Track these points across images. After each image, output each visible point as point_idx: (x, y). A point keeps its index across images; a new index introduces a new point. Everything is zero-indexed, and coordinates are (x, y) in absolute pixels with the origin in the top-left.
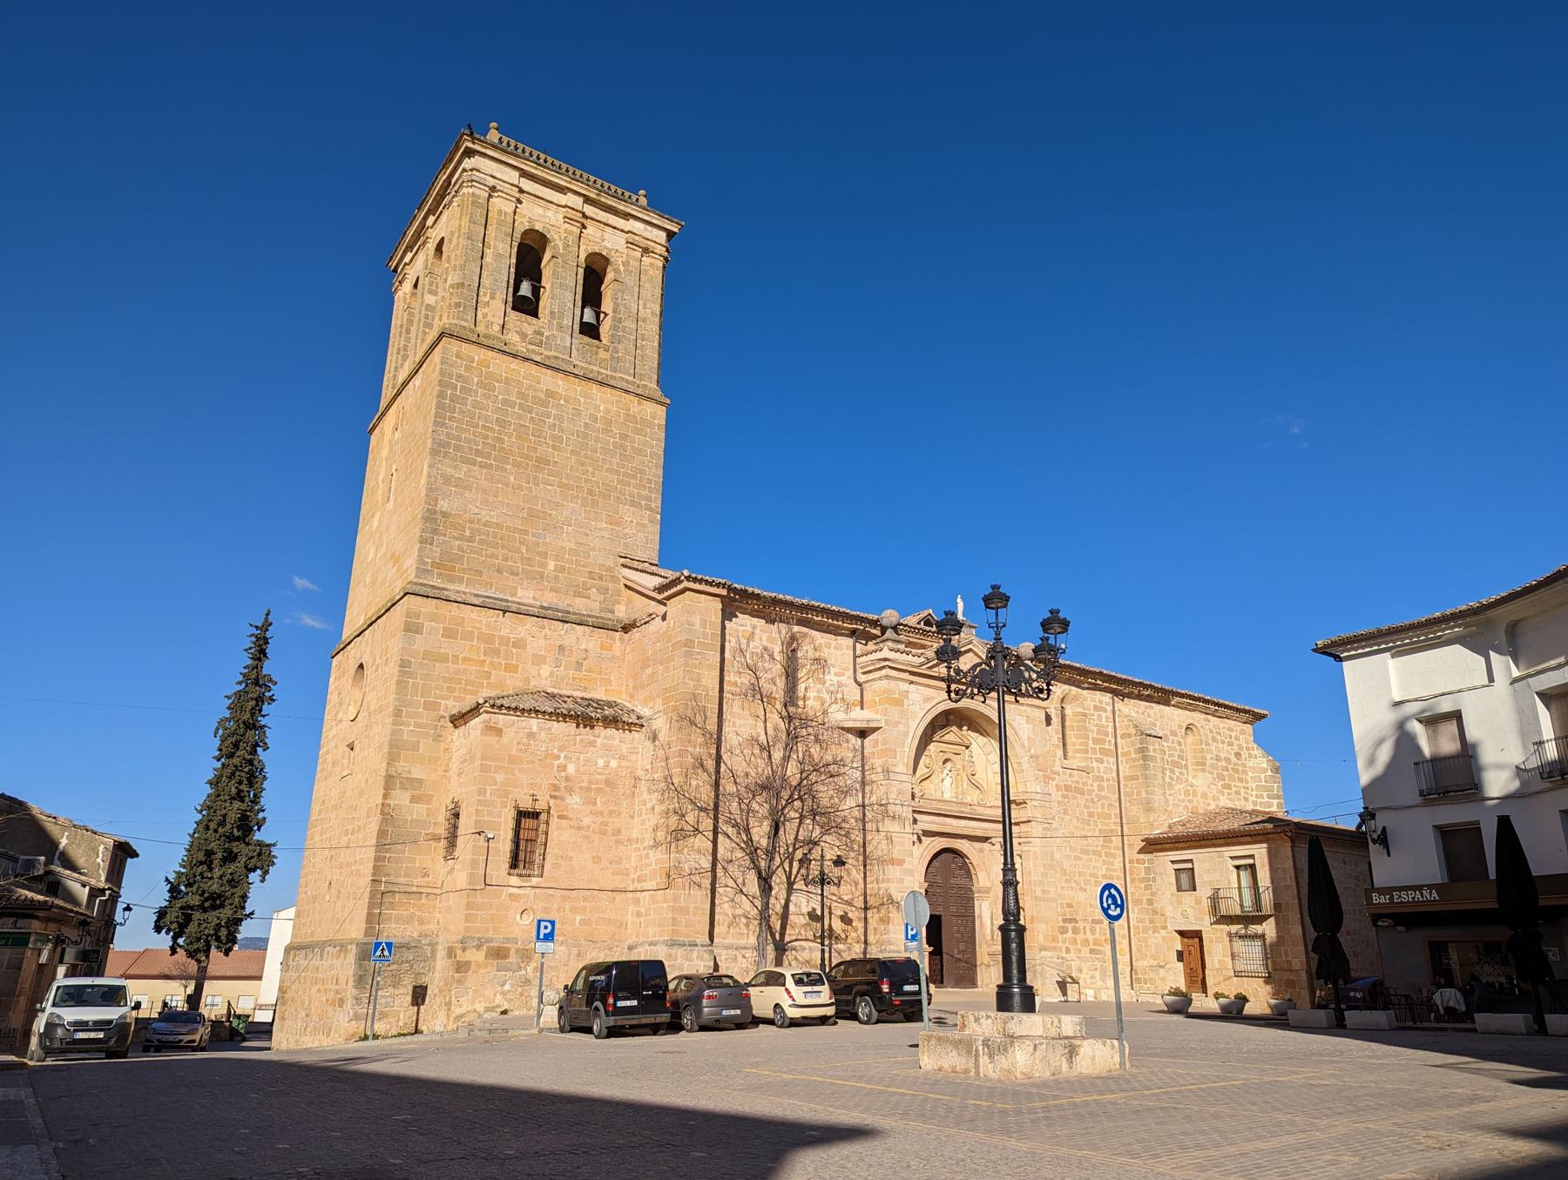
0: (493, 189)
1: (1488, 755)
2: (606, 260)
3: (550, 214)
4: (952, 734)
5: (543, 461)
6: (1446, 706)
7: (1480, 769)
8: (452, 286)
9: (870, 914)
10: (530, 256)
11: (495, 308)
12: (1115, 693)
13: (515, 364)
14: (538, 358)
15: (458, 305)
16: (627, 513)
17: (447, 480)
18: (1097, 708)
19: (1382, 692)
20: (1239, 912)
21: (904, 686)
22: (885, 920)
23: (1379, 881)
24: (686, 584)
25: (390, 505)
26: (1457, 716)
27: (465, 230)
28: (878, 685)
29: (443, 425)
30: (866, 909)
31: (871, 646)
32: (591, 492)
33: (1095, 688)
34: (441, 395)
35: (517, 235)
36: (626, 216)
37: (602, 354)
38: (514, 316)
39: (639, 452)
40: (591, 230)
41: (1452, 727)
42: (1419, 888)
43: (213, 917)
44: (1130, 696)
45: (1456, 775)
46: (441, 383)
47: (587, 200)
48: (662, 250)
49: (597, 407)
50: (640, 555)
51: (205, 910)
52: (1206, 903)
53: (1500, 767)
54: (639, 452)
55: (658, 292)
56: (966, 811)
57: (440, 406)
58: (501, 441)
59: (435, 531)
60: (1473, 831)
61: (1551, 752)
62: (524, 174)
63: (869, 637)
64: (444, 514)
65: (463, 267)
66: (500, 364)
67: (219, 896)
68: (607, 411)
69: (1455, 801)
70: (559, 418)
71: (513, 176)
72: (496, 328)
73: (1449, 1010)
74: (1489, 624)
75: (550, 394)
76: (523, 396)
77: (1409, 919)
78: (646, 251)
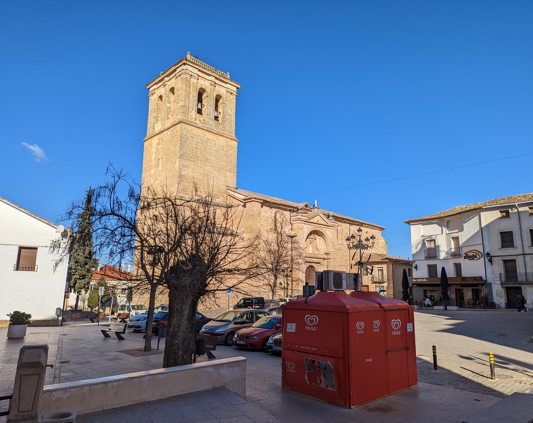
0: (191, 75)
1: (441, 249)
2: (221, 97)
3: (206, 83)
4: (312, 236)
5: (207, 159)
6: (433, 238)
7: (439, 251)
8: (181, 106)
9: (293, 282)
10: (201, 94)
11: (194, 113)
12: (350, 224)
13: (199, 130)
14: (205, 128)
15: (184, 112)
16: (228, 174)
17: (184, 166)
18: (346, 228)
19: (418, 233)
20: (378, 281)
21: (303, 225)
22: (298, 284)
23: (414, 276)
24: (253, 200)
25: (160, 168)
26: (434, 240)
27: (184, 89)
28: (296, 225)
29: (182, 149)
30: (292, 281)
31: (294, 214)
32: (219, 168)
33: (345, 222)
34: (181, 140)
35: (198, 90)
36: (226, 83)
37: (221, 126)
38: (198, 115)
39: (231, 156)
40: (217, 88)
41: (433, 242)
42: (423, 279)
43: (83, 281)
44: (353, 224)
45: (432, 253)
46: (181, 137)
47: (216, 78)
48: (235, 93)
49: (220, 143)
50: (232, 186)
51: (80, 279)
52: (370, 278)
53: (443, 251)
54: (231, 156)
55: (235, 106)
56: (315, 256)
57: (181, 144)
58: (196, 153)
59: (181, 181)
60: (435, 266)
61: (453, 250)
62: (199, 70)
63: (294, 211)
64: (184, 176)
65: (184, 101)
66: (196, 131)
67: (84, 275)
68: (223, 144)
69: (432, 259)
70: (211, 146)
71: (196, 71)
72: (194, 119)
73: (428, 305)
74: (443, 220)
75: (208, 139)
76: (201, 140)
77: (420, 285)
78: (231, 93)
